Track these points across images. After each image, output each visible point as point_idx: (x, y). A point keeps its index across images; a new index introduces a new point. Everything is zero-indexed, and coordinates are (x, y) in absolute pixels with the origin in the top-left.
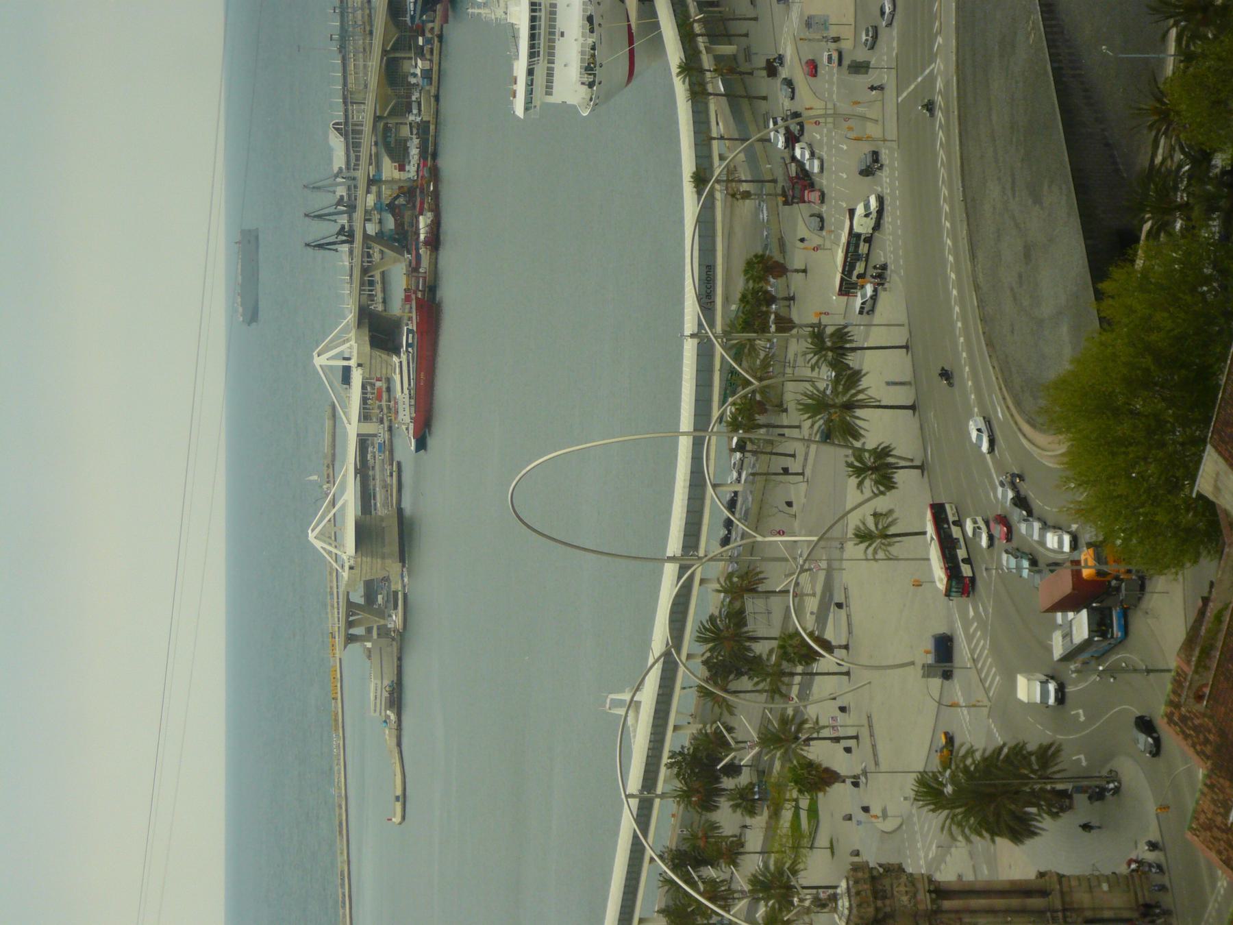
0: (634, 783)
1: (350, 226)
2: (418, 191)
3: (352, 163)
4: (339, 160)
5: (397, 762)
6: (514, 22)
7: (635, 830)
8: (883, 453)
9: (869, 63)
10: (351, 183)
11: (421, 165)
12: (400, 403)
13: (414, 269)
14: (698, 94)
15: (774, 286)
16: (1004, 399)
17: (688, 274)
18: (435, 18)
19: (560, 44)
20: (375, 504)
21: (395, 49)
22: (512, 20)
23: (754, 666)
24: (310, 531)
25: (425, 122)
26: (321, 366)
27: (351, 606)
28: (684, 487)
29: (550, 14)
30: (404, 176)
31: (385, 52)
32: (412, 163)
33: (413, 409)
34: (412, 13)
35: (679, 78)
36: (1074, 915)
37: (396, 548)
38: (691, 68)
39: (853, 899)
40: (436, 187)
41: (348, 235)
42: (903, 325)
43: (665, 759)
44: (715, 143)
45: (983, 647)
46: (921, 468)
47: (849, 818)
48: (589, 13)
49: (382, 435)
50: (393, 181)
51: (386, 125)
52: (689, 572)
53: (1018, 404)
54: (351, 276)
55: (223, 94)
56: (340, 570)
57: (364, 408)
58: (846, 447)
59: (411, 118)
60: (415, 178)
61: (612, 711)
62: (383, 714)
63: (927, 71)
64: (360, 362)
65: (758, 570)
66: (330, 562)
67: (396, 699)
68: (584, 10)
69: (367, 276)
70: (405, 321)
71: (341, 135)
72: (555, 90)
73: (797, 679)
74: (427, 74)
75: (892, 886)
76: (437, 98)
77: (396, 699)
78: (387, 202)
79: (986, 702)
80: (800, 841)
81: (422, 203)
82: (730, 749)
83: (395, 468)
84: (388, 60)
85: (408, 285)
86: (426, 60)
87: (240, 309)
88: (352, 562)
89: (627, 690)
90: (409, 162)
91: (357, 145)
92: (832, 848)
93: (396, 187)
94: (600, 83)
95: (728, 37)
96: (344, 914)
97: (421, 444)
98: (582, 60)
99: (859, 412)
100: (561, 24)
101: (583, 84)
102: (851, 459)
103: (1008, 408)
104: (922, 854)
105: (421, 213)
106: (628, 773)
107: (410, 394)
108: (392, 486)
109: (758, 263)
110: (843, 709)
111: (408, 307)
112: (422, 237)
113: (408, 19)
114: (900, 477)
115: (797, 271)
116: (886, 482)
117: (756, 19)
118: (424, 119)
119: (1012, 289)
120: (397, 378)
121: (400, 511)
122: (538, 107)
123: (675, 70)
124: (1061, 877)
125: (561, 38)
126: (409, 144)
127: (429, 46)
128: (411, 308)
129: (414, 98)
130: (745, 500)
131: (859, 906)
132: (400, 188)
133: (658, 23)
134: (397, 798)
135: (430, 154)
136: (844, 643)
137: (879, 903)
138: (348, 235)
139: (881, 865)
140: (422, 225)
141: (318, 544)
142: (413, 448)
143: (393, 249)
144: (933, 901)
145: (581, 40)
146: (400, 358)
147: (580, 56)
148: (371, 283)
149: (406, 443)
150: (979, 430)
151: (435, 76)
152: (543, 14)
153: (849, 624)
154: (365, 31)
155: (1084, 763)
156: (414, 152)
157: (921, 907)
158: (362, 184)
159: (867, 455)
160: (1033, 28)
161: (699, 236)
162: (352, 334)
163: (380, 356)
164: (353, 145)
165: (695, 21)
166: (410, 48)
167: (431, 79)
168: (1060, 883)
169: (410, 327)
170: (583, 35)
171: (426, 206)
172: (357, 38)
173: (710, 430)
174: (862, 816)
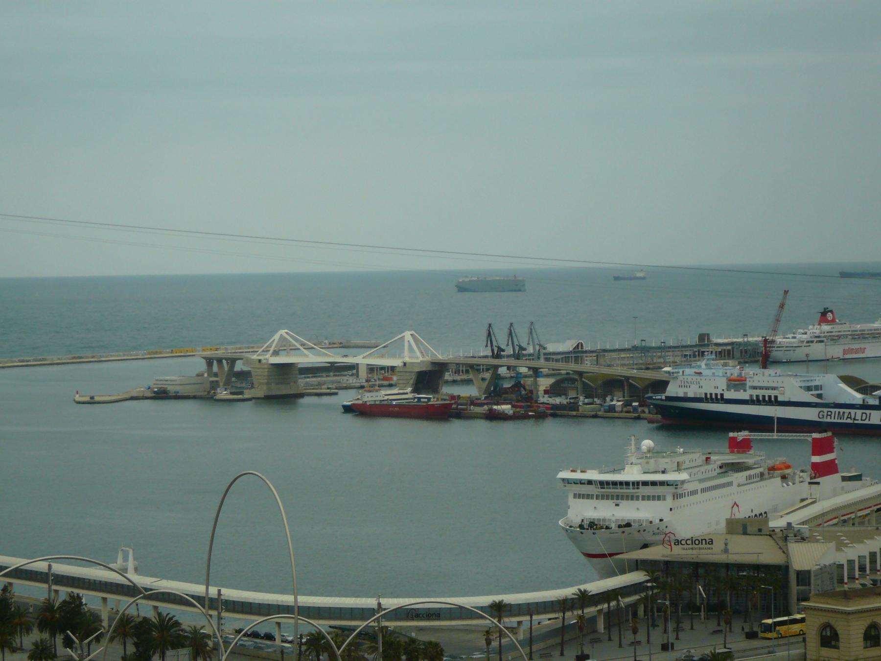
0: (60, 568)
2: (529, 404)
3: (549, 357)
4: (551, 348)
5: (120, 397)
6: (626, 470)
7: (9, 567)
11: (548, 406)
13: (473, 402)
14: (564, 605)
18: (652, 414)
19: (610, 503)
20: (309, 377)
21: (630, 385)
22: (627, 468)
24: (286, 331)
25: (578, 408)
27: (232, 361)
28: (277, 601)
29: (636, 496)
30: (541, 393)
31: (627, 378)
33: (373, 403)
34: (654, 397)
35: (577, 591)
37: (274, 393)
38: (584, 599)
41: (498, 354)
43: (76, 591)
44: (528, 618)
48: (632, 524)
49: (358, 381)
50: (536, 384)
51: (576, 380)
54: (473, 357)
56: (258, 353)
57: (377, 368)
59: (582, 398)
60: (539, 402)
61: (120, 551)
62: (155, 386)
64: (407, 365)
65: (212, 656)
66: (263, 346)
67: (161, 395)
68: (635, 521)
70: (436, 396)
71: (574, 349)
72: (577, 500)
74: (612, 409)
76: (595, 416)
77: (161, 395)
78: (522, 382)
81: (520, 407)
82: (81, 640)
84: (620, 381)
85: (462, 397)
86: (622, 408)
87: (467, 280)
88: (264, 361)
89: (136, 562)
90: (550, 397)
93: (533, 388)
94: (582, 533)
95: (608, 627)
97: (348, 409)
98: (599, 520)
100: (624, 503)
101: (583, 521)
105: (513, 406)
107: (383, 400)
108: (321, 389)
109: (437, 652)
111: (448, 398)
112: (495, 407)
113: (650, 395)
117: (620, 646)
118: (580, 407)
121: (302, 395)
122: (565, 488)
123: (583, 587)
125: (614, 504)
127: (632, 410)
129: (596, 400)
130: (268, 647)
133: (625, 573)
134: (92, 398)
135: (556, 412)
138: (498, 354)
141: (276, 337)
142: (345, 403)
143: (488, 387)
145: (613, 519)
147: (602, 518)
148: (467, 372)
149: (348, 398)
151: (610, 414)
152: (631, 491)
154: (649, 364)
156: (557, 400)
158: (534, 364)
162: (428, 359)
163: (412, 379)
164: (566, 357)
165: (618, 601)
166: (631, 396)
167: (609, 412)
169: (432, 400)
170: (617, 520)
171: (518, 410)
172: (644, 358)
173: (299, 617)
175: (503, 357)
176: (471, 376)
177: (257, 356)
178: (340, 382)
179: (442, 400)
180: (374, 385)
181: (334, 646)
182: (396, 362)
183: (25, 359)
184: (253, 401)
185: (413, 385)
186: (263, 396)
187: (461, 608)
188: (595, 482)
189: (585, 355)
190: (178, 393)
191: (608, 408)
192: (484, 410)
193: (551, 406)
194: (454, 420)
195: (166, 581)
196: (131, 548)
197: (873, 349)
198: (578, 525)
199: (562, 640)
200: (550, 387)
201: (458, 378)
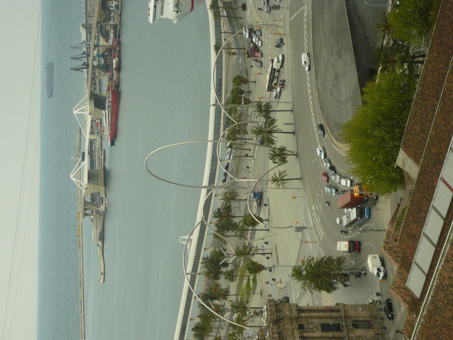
0: (189, 269)
1: (88, 62)
3: (88, 38)
4: (84, 37)
7: (189, 286)
8: (282, 150)
9: (280, 6)
13: (111, 79)
14: (217, 16)
15: (244, 87)
20: (95, 165)
23: (234, 226)
24: (71, 175)
27: (86, 203)
30: (108, 44)
32: (111, 39)
33: (110, 130)
36: (349, 319)
41: (86, 65)
42: (290, 103)
43: (201, 260)
45: (318, 221)
46: (296, 155)
49: (98, 140)
50: (104, 46)
51: (101, 25)
52: (211, 192)
54: (88, 81)
58: (269, 147)
59: (111, 23)
62: (97, 242)
67: (102, 237)
69: (93, 81)
72: (164, 14)
73: (250, 232)
74: (117, 6)
76: (120, 15)
77: (102, 237)
79: (318, 241)
80: (250, 291)
85: (108, 84)
88: (86, 187)
90: (110, 39)
91: (90, 32)
92: (261, 294)
93: (105, 48)
94: (181, 11)
96: (82, 316)
97: (113, 143)
98: (174, 3)
99: (274, 134)
101: (174, 11)
105: (114, 58)
106: (187, 262)
107: (109, 125)
108: (101, 158)
109: (238, 79)
110: (266, 243)
112: (114, 67)
114: (289, 158)
115: (252, 82)
116: (284, 161)
118: (116, 23)
119: (331, 90)
120: (104, 119)
121: (104, 168)
122: (158, 20)
123: (208, 7)
124: (344, 305)
129: (112, 15)
131: (271, 315)
134: (102, 274)
135: (117, 36)
136: (267, 219)
137: (278, 314)
138: (86, 65)
139: (279, 300)
141: (74, 180)
142: (110, 145)
143: (104, 71)
144: (298, 313)
146: (105, 111)
148: (95, 84)
149: (107, 143)
151: (120, 7)
155: (354, 264)
156: (112, 35)
157: (293, 315)
158: (92, 47)
161: (217, 68)
162: (88, 102)
163: (98, 111)
164: (89, 32)
168: (344, 307)
169: (109, 100)
171: (116, 55)
174: (272, 282)
175: (88, 62)
176: (97, 81)
177: (83, 190)
178: (98, 149)
179: (109, 94)
180: (101, 130)
181: (222, 237)
182: (89, 119)
183: (80, 310)
184: (107, 192)
185: (101, 110)
186: (104, 187)
187: (205, 204)
188: (155, 3)
189: (88, 23)
190: (101, 231)
191: (116, 9)
192: (116, 73)
193: (114, 38)
194: (120, 89)
195: (197, 218)
196: (180, 237)
197: (83, 339)
198: (177, 14)
199: (234, 17)
200: (105, 39)
201: (98, 88)
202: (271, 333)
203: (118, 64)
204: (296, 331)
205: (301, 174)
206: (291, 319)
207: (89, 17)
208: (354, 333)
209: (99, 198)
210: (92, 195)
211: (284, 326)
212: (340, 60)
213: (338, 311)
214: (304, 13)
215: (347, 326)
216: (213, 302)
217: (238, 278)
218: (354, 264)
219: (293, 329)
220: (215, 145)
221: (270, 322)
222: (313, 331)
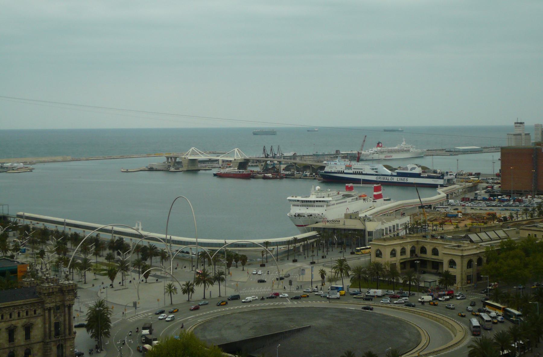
0: (116, 229)
1: (269, 157)
3: (284, 158)
4: (285, 154)
10: (280, 158)
12: (225, 170)
13: (258, 173)
14: (289, 243)
15: (240, 263)
16: (450, 319)
17: (237, 241)
19: (305, 208)
26: (235, 150)
27: (176, 158)
30: (282, 170)
31: (311, 165)
32: (285, 172)
33: (224, 173)
36: (64, 342)
38: (296, 241)
39: (68, 285)
40: (278, 178)
42: (226, 295)
43: (122, 236)
44: (276, 247)
45: (140, 317)
46: (189, 300)
47: (103, 283)
48: (313, 215)
50: (280, 167)
51: (294, 166)
52: (163, 241)
53: (200, 325)
55: (304, 126)
58: (194, 282)
59: (296, 172)
63: (288, 300)
67: (151, 169)
68: (313, 214)
69: (258, 161)
71: (293, 155)
73: (138, 269)
74: (306, 176)
75: (71, 295)
76: (300, 178)
77: (151, 169)
78: (275, 166)
79: (126, 318)
80: (97, 271)
81: (275, 175)
82: (123, 253)
83: (210, 169)
85: (255, 171)
87: (257, 131)
88: (186, 158)
91: (291, 159)
92: (96, 279)
94: (295, 218)
95: (304, 250)
96: (101, 158)
97: (215, 175)
99: (203, 285)
100: (310, 208)
102: (190, 283)
103: (200, 322)
104: (90, 302)
106: (117, 227)
108: (206, 168)
109: (245, 258)
110: (130, 282)
112: (266, 175)
113: (319, 171)
114: (186, 295)
115: (243, 268)
116: (185, 292)
119: (230, 323)
120: (232, 169)
121: (199, 170)
123: (295, 237)
124: (74, 338)
126: (289, 171)
128: (249, 172)
129: (300, 172)
130: (187, 256)
131: (66, 286)
132: (278, 169)
133: (310, 232)
134: (127, 170)
135: (287, 177)
136: (147, 281)
137: (66, 291)
139: (77, 291)
140: (269, 175)
141: (191, 150)
142: (214, 173)
144: (67, 305)
145: (306, 213)
146: (237, 169)
149: (215, 171)
150: (164, 316)
151: (305, 177)
153: (152, 283)
155: (106, 344)
156: (287, 173)
157: (66, 302)
158: (279, 160)
159: (192, 287)
160: (294, 327)
161: (250, 244)
162: (243, 158)
164: (290, 158)
166: (312, 171)
168: (72, 338)
171: (274, 176)
174: (102, 286)
175: (269, 157)
176: (258, 164)
182: (232, 159)
188: (300, 200)
201: (253, 165)
202: (52, 287)
203: (268, 177)
204: (54, 304)
205: (175, 304)
206: (63, 301)
207: (301, 157)
208: (54, 346)
209: (179, 167)
210: (181, 162)
211: (58, 296)
212: (250, 329)
213: (70, 334)
214: (286, 302)
215: (59, 340)
216: (94, 246)
217: (108, 262)
218: (106, 344)
219: (56, 302)
220: (193, 243)
221: (61, 286)
222: (55, 316)
